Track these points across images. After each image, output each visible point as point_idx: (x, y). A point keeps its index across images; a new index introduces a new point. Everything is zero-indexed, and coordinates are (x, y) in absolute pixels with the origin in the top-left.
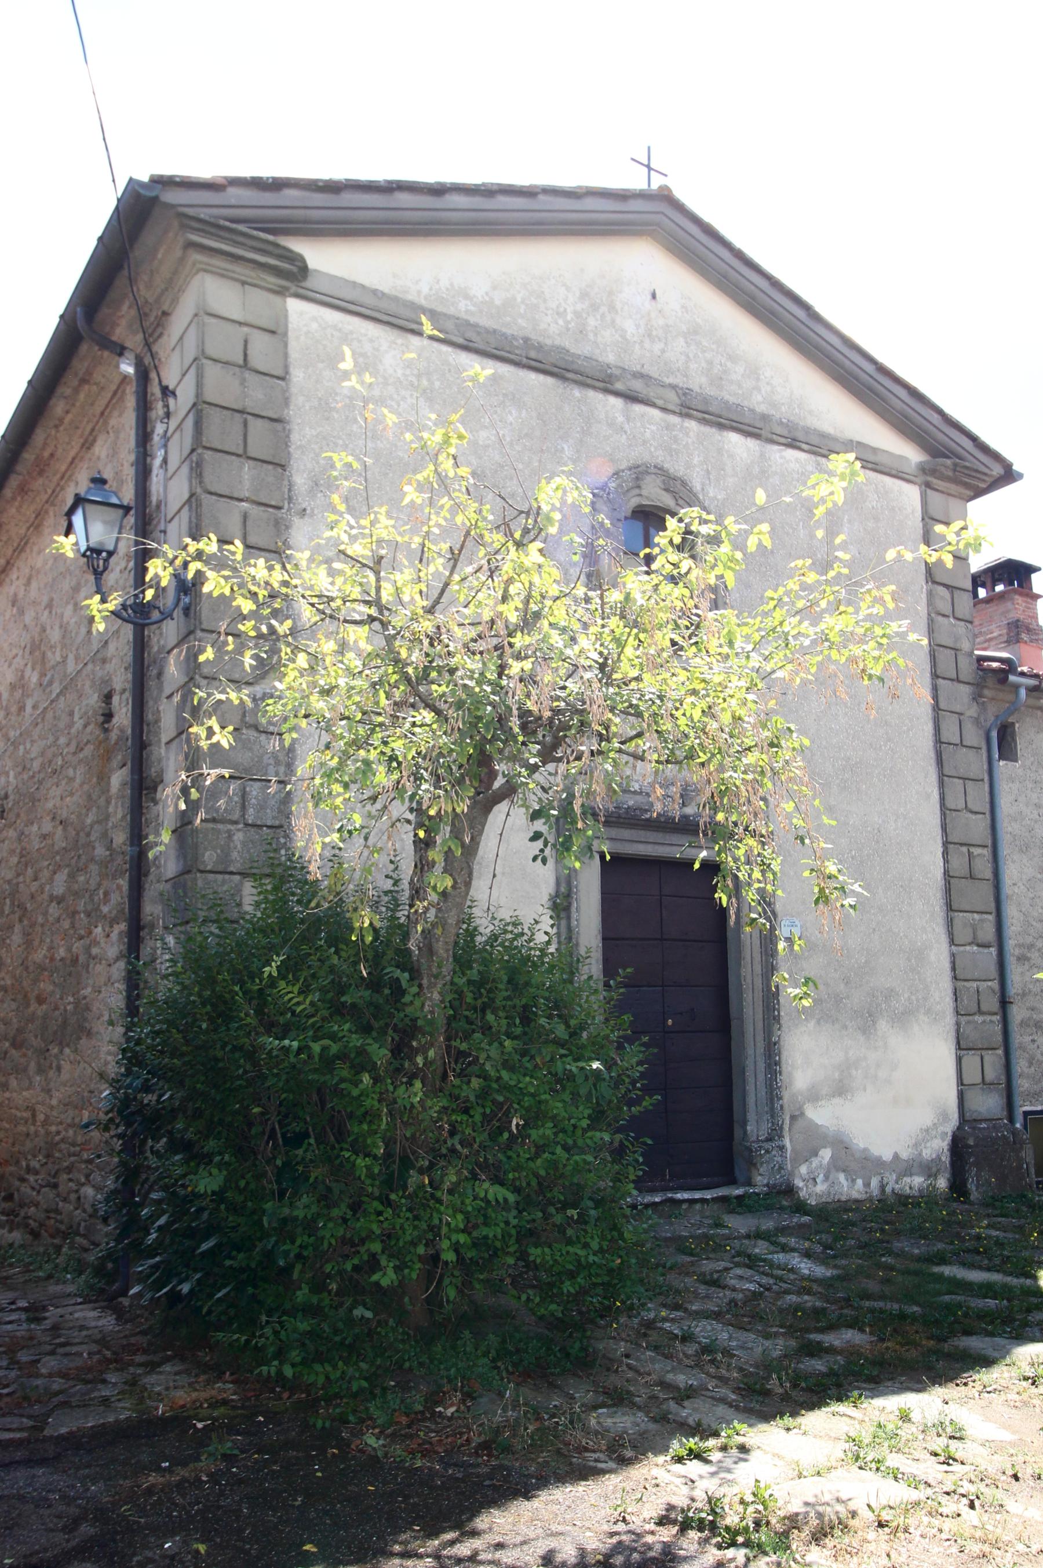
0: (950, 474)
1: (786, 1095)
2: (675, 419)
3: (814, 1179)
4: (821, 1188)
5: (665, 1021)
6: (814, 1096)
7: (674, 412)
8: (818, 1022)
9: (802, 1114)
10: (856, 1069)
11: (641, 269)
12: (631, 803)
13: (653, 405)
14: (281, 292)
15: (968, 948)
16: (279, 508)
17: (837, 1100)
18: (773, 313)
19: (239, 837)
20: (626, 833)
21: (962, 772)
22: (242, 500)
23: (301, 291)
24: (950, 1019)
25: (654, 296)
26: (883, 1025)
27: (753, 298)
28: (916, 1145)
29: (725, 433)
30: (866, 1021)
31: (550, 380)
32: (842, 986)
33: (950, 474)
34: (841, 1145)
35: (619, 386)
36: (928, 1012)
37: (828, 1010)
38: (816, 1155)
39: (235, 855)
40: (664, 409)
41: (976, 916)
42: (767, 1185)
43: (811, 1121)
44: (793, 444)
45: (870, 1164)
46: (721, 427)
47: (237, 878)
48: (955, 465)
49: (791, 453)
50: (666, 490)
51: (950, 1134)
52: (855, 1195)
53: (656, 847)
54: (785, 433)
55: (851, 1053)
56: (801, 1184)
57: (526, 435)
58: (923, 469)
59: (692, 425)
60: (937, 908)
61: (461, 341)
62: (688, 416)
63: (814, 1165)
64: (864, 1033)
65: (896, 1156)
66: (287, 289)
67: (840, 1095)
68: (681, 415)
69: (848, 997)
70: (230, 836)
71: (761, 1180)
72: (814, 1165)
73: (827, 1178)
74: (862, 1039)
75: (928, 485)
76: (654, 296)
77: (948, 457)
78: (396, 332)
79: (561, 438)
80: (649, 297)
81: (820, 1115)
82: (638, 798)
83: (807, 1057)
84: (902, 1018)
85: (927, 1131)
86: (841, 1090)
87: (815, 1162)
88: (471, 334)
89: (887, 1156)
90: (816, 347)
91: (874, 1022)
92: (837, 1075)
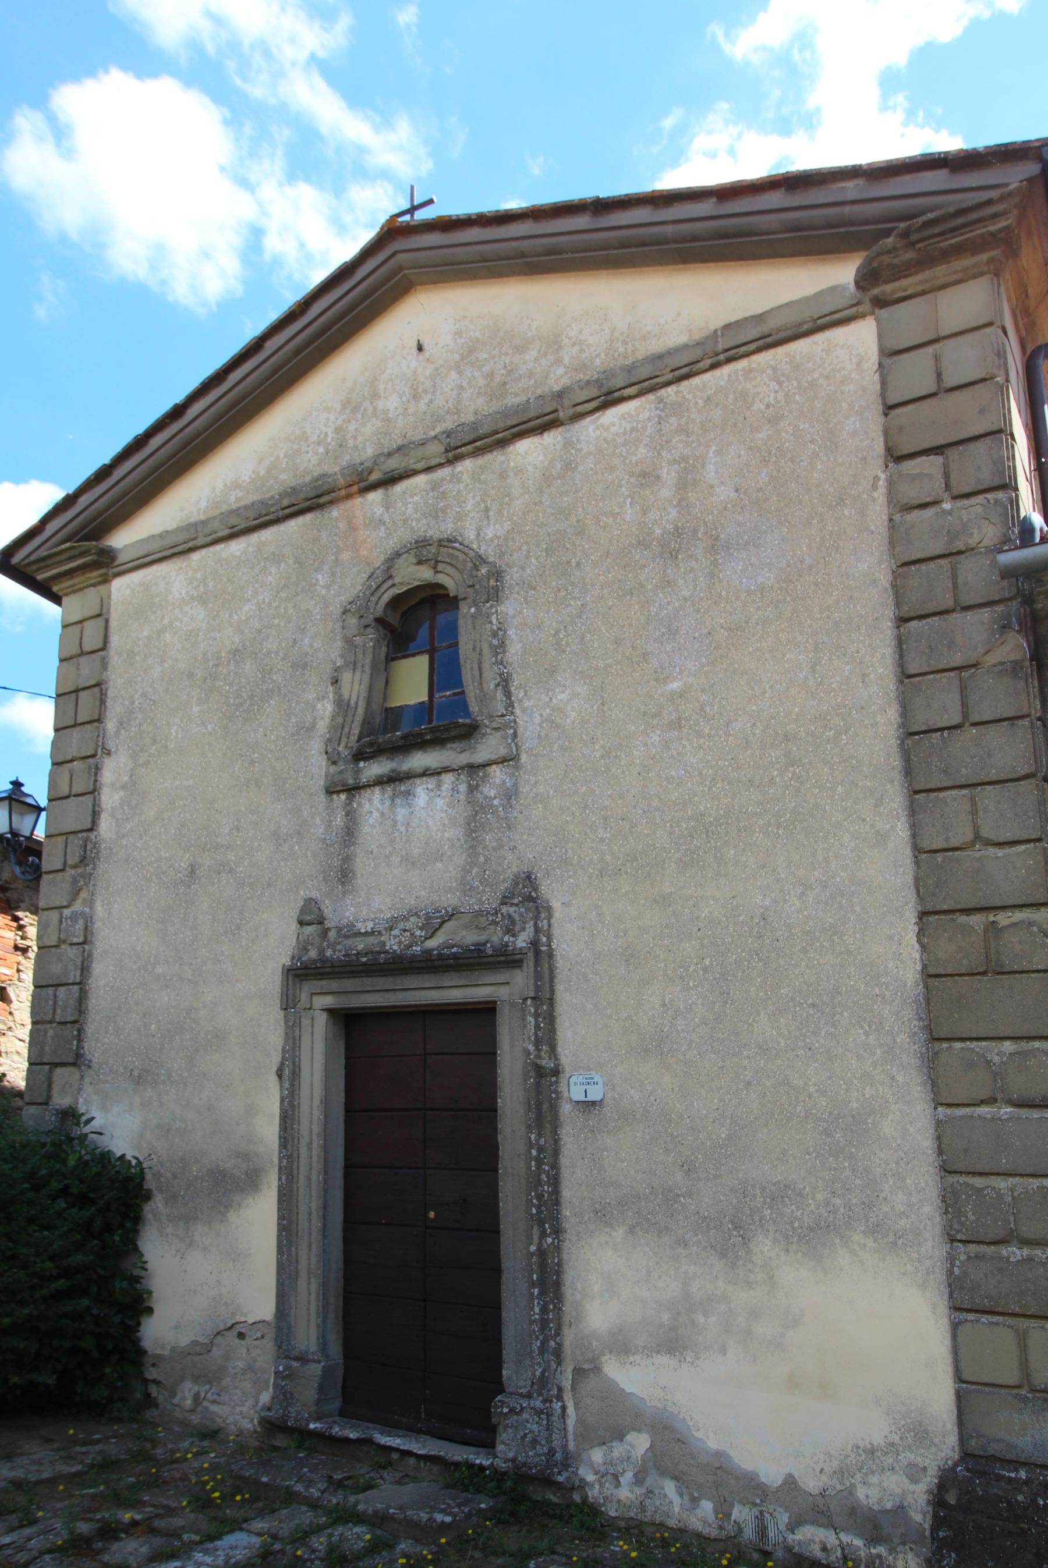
0: (910, 255)
1: (569, 1338)
2: (445, 472)
3: (616, 1477)
4: (626, 1492)
5: (426, 1213)
6: (622, 1346)
7: (440, 465)
8: (631, 1230)
9: (597, 1369)
10: (706, 1315)
11: (430, 320)
12: (360, 947)
13: (415, 473)
14: (106, 580)
15: (984, 1110)
16: (93, 756)
17: (663, 1360)
18: (551, 252)
19: (50, 1033)
20: (349, 984)
21: (965, 774)
22: (72, 761)
23: (116, 570)
24: (932, 1247)
25: (420, 348)
26: (764, 1246)
27: (522, 255)
28: (840, 1473)
29: (511, 448)
30: (730, 1235)
31: (308, 517)
32: (679, 1176)
33: (910, 255)
34: (668, 1433)
35: (375, 477)
36: (876, 1230)
37: (652, 1212)
38: (621, 1438)
39: (47, 1048)
40: (428, 469)
41: (1008, 1046)
42: (514, 1460)
43: (613, 1383)
44: (609, 399)
45: (722, 1479)
46: (503, 443)
47: (47, 1067)
48: (905, 234)
49: (612, 415)
50: (420, 563)
51: (933, 1472)
52: (695, 1523)
53: (388, 995)
54: (594, 392)
55: (695, 1286)
56: (590, 1478)
57: (284, 586)
58: (866, 279)
59: (467, 466)
60: (903, 1038)
61: (227, 532)
62: (458, 458)
63: (616, 1454)
64: (723, 1255)
65: (790, 1482)
66: (106, 574)
67: (671, 1351)
68: (450, 462)
69: (690, 1194)
70: (46, 1032)
71: (507, 1450)
72: (616, 1454)
73: (639, 1480)
74: (719, 1265)
75: (880, 303)
76: (420, 348)
77: (887, 233)
78: (182, 558)
79: (316, 570)
80: (425, 347)
81: (633, 1378)
82: (371, 940)
83: (611, 1285)
84: (813, 1237)
85: (872, 1452)
86: (673, 1342)
87: (618, 1450)
88: (234, 520)
89: (771, 1475)
90: (623, 246)
91: (746, 1240)
92: (666, 1317)
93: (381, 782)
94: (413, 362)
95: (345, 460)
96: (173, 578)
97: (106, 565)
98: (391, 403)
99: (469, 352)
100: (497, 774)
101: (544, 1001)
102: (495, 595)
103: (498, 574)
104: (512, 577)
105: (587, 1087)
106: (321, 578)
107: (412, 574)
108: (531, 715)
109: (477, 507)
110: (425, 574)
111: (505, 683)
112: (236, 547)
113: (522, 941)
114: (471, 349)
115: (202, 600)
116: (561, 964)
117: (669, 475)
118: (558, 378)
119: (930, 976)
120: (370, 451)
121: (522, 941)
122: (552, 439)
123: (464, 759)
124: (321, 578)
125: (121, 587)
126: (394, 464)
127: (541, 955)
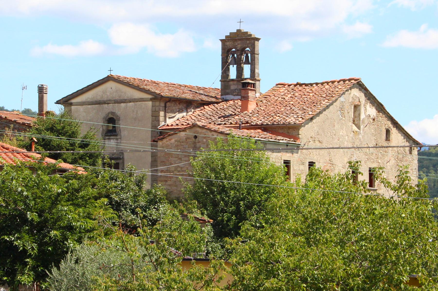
11: (110, 85)
44: (130, 102)
49: (130, 103)
59: (116, 104)
93: (108, 139)
94: (111, 90)
95: (103, 99)
96: (81, 108)
97: (71, 104)
98: (108, 94)
99: (117, 91)
100: (119, 140)
101: (123, 163)
102: (119, 120)
103: (119, 118)
104: (121, 118)
105: (385, 144)
106: (100, 113)
107: (110, 116)
108: (122, 134)
109: (119, 110)
110: (112, 116)
111: (120, 130)
112: (89, 106)
113: (121, 157)
114: (117, 91)
115: (85, 112)
116: (125, 159)
117: (135, 111)
118: (126, 98)
119: (152, 161)
120: (106, 99)
121: (121, 157)
122: (125, 104)
123: (116, 138)
124: (100, 113)
125: (72, 107)
126: (108, 102)
127: (123, 158)
